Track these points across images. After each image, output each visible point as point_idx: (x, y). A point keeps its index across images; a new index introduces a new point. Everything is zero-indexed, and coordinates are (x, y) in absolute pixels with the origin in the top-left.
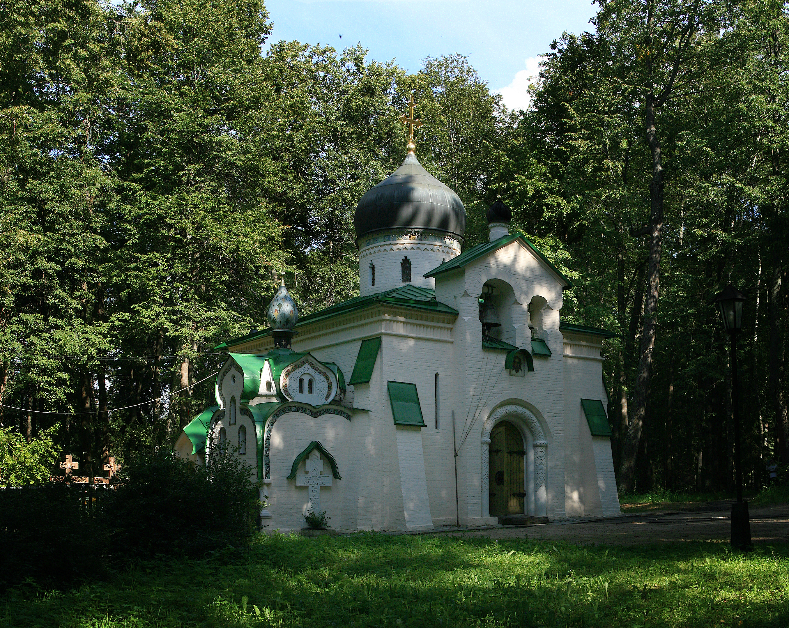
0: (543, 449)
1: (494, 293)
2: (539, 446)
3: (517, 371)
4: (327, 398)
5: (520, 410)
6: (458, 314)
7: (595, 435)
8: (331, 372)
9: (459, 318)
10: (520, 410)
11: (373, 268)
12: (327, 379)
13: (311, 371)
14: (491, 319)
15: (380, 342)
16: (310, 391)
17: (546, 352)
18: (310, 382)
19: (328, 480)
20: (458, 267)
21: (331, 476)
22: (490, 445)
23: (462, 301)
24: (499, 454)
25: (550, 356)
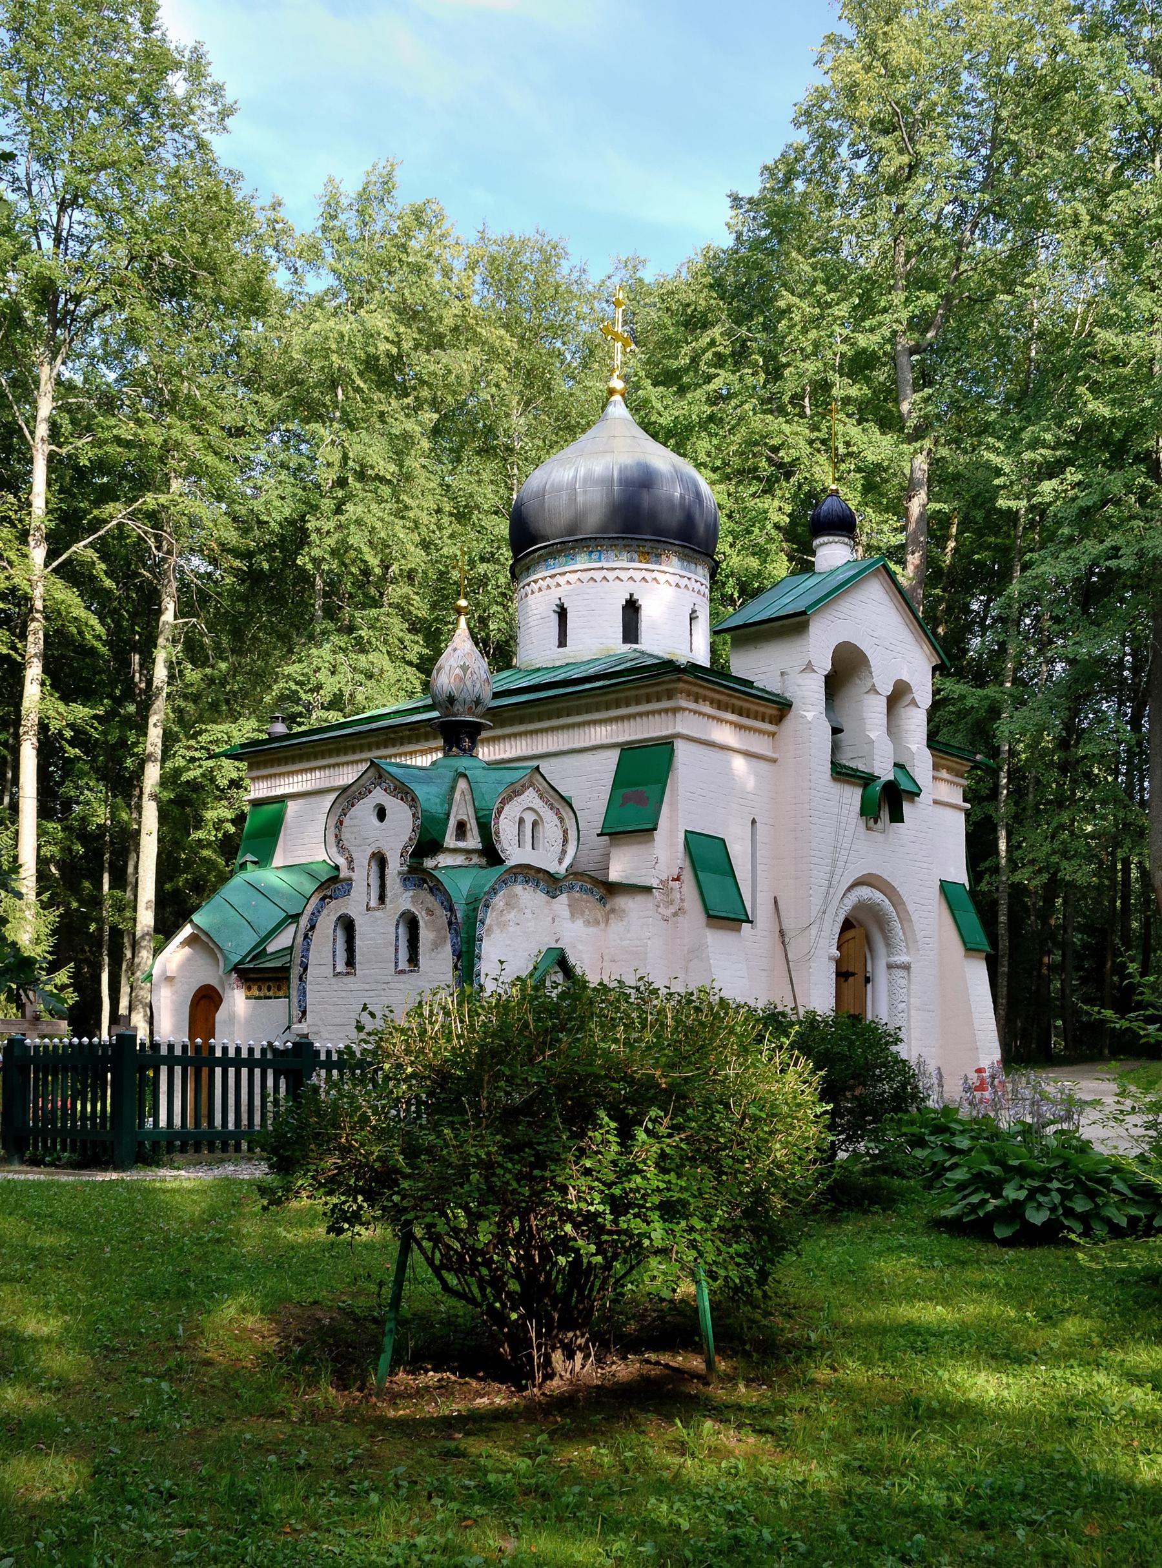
0: (903, 973)
2: (898, 967)
3: (876, 822)
5: (878, 896)
6: (790, 706)
7: (970, 950)
8: (568, 809)
9: (791, 715)
10: (878, 896)
11: (562, 613)
12: (562, 820)
13: (537, 803)
15: (673, 750)
17: (916, 790)
18: (535, 824)
20: (804, 613)
22: (838, 962)
23: (800, 681)
24: (851, 979)
25: (918, 795)
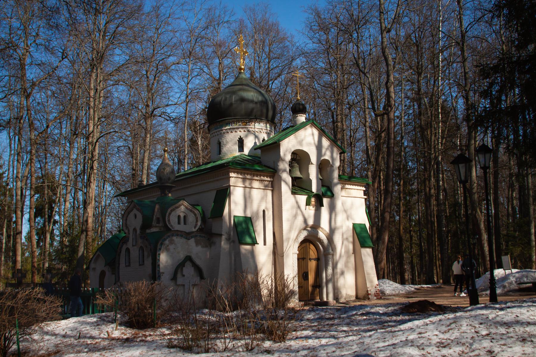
1: (298, 158)
4: (195, 227)
14: (298, 174)
16: (185, 223)
19: (197, 280)
21: (199, 278)
